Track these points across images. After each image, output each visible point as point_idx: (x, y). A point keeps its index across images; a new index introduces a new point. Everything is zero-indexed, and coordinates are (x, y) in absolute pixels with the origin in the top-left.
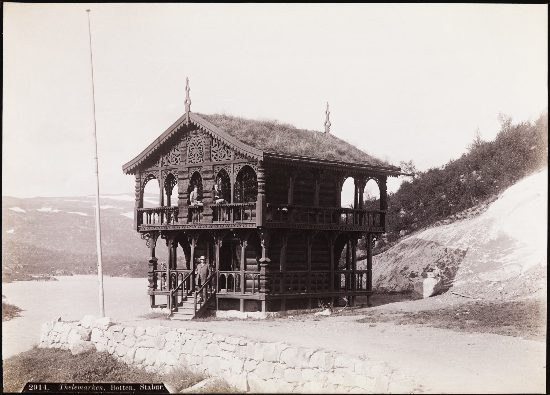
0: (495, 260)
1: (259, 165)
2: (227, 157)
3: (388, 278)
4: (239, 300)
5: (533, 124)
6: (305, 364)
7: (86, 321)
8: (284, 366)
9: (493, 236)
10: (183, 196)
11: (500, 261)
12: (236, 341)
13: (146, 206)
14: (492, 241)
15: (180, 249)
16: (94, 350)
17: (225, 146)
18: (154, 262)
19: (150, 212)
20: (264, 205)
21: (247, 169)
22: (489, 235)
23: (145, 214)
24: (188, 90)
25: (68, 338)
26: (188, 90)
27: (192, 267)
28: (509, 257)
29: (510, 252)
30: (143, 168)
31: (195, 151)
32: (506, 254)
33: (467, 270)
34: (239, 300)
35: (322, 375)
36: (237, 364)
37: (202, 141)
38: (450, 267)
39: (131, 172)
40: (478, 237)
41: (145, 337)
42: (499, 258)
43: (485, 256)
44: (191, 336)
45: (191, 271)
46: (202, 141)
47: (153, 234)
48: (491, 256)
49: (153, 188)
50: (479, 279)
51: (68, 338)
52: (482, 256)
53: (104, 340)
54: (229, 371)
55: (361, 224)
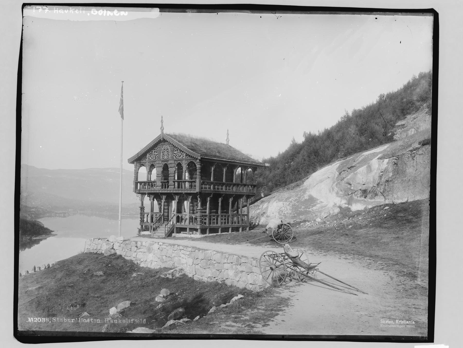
0: (308, 210)
1: (198, 161)
2: (181, 157)
3: (255, 218)
4: (186, 228)
5: (292, 143)
6: (225, 261)
7: (111, 239)
8: (215, 262)
9: (306, 197)
10: (159, 175)
11: (310, 210)
12: (190, 249)
13: (139, 180)
14: (306, 200)
15: (156, 202)
16: (116, 253)
17: (181, 151)
18: (142, 208)
19: (141, 183)
20: (200, 181)
21: (192, 163)
22: (304, 197)
23: (139, 184)
24: (162, 121)
25: (101, 247)
26: (162, 121)
27: (162, 212)
28: (314, 208)
29: (315, 205)
30: (139, 160)
31: (166, 153)
32: (313, 206)
33: (294, 214)
34: (186, 228)
35: (234, 266)
36: (190, 261)
37: (169, 148)
38: (286, 212)
39: (133, 162)
40: (299, 198)
41: (142, 247)
42: (309, 208)
43: (303, 207)
44: (165, 247)
45: (162, 214)
46: (169, 148)
47: (143, 194)
48: (306, 208)
49: (143, 171)
50: (300, 219)
51: (101, 247)
52: (301, 207)
53: (121, 249)
54: (185, 265)
55: (182, 188)
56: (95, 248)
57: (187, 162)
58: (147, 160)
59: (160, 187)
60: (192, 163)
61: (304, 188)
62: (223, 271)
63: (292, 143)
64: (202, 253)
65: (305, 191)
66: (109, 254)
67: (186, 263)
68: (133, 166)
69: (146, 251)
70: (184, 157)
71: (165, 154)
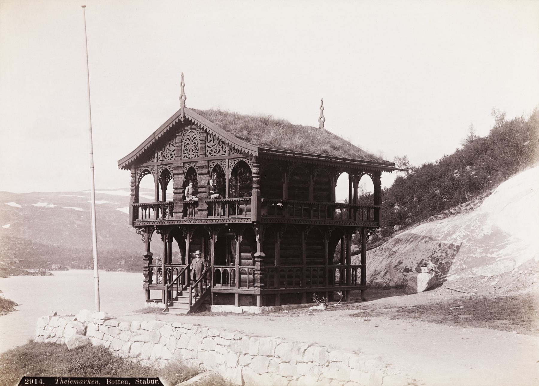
0: (489, 255)
1: (254, 160)
3: (383, 273)
5: (527, 119)
6: (299, 358)
7: (82, 316)
8: (279, 361)
10: (178, 191)
11: (494, 255)
12: (231, 335)
13: (141, 202)
14: (486, 236)
15: (175, 244)
16: (90, 344)
17: (220, 141)
18: (149, 257)
19: (145, 207)
20: (259, 200)
22: (482, 230)
23: (140, 209)
24: (183, 85)
25: (63, 333)
27: (187, 262)
29: (504, 247)
30: (138, 163)
31: (190, 147)
32: (500, 248)
33: (461, 265)
35: (316, 369)
36: (232, 358)
37: (197, 136)
38: (444, 262)
39: (127, 167)
40: (472, 232)
42: (492, 253)
43: (479, 250)
46: (197, 136)
47: (148, 229)
48: (485, 251)
49: (148, 183)
51: (63, 333)
52: (476, 251)
53: (100, 335)
54: (223, 366)
55: (355, 219)
56: (52, 335)
57: (233, 164)
58: (155, 160)
59: (181, 215)
60: (242, 164)
61: (481, 213)
62: (295, 378)
63: (527, 119)
64: (256, 340)
65: (483, 218)
66: (77, 344)
67: (225, 363)
68: (128, 173)
69: (147, 339)
70: (227, 154)
71: (188, 145)
